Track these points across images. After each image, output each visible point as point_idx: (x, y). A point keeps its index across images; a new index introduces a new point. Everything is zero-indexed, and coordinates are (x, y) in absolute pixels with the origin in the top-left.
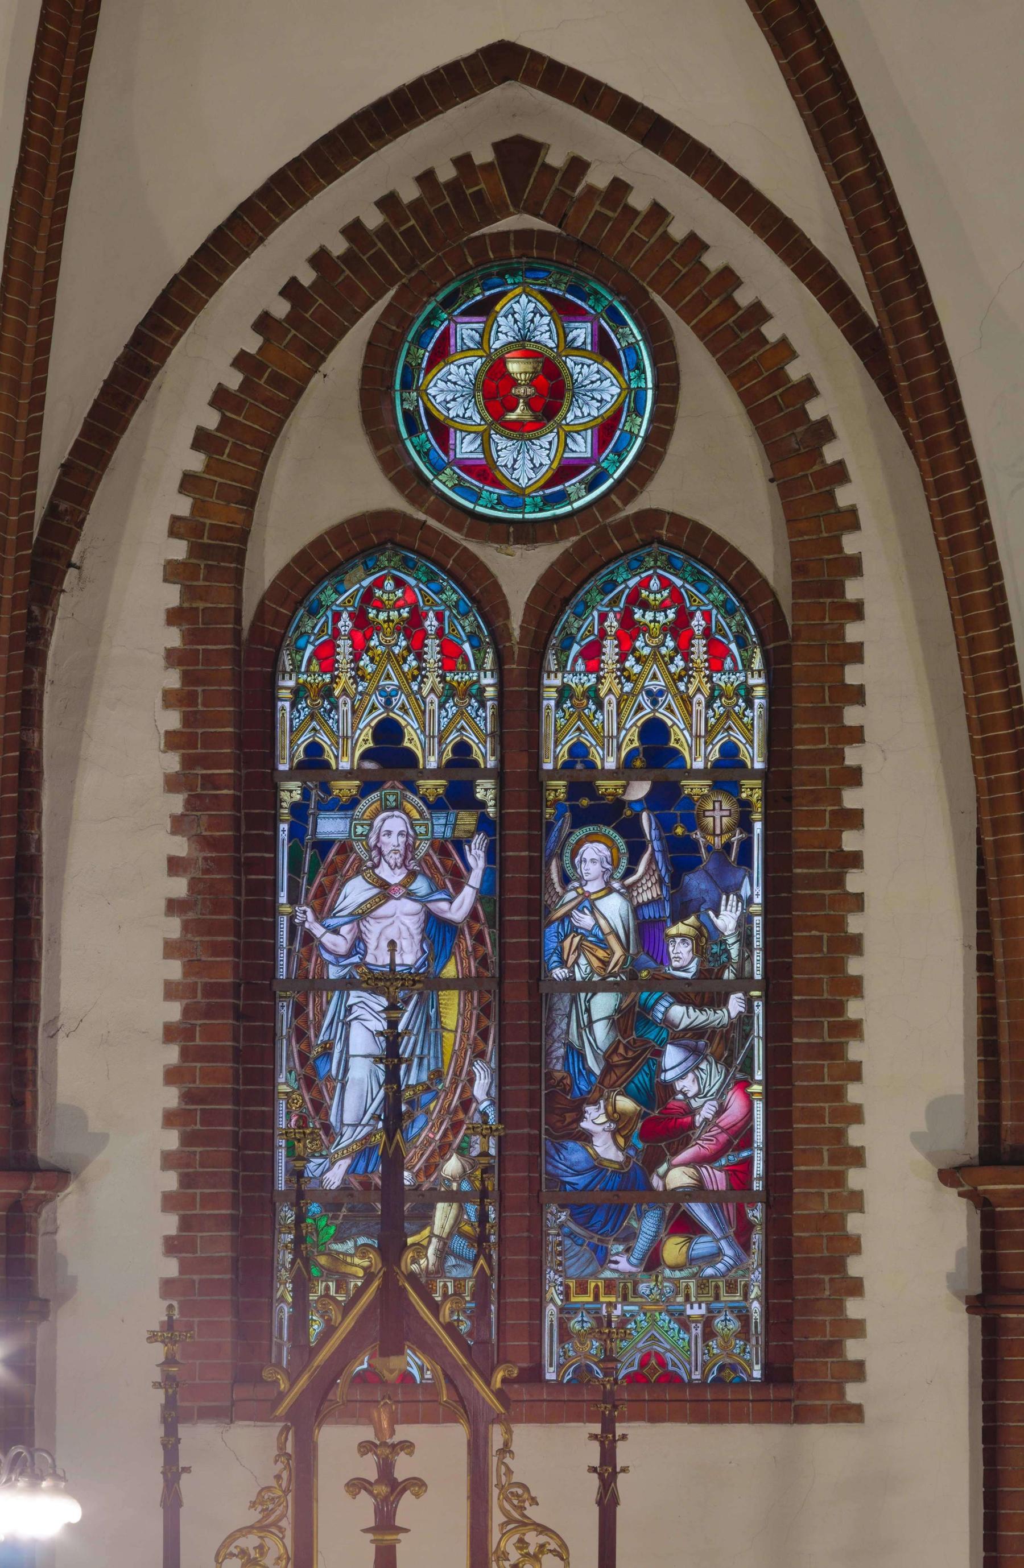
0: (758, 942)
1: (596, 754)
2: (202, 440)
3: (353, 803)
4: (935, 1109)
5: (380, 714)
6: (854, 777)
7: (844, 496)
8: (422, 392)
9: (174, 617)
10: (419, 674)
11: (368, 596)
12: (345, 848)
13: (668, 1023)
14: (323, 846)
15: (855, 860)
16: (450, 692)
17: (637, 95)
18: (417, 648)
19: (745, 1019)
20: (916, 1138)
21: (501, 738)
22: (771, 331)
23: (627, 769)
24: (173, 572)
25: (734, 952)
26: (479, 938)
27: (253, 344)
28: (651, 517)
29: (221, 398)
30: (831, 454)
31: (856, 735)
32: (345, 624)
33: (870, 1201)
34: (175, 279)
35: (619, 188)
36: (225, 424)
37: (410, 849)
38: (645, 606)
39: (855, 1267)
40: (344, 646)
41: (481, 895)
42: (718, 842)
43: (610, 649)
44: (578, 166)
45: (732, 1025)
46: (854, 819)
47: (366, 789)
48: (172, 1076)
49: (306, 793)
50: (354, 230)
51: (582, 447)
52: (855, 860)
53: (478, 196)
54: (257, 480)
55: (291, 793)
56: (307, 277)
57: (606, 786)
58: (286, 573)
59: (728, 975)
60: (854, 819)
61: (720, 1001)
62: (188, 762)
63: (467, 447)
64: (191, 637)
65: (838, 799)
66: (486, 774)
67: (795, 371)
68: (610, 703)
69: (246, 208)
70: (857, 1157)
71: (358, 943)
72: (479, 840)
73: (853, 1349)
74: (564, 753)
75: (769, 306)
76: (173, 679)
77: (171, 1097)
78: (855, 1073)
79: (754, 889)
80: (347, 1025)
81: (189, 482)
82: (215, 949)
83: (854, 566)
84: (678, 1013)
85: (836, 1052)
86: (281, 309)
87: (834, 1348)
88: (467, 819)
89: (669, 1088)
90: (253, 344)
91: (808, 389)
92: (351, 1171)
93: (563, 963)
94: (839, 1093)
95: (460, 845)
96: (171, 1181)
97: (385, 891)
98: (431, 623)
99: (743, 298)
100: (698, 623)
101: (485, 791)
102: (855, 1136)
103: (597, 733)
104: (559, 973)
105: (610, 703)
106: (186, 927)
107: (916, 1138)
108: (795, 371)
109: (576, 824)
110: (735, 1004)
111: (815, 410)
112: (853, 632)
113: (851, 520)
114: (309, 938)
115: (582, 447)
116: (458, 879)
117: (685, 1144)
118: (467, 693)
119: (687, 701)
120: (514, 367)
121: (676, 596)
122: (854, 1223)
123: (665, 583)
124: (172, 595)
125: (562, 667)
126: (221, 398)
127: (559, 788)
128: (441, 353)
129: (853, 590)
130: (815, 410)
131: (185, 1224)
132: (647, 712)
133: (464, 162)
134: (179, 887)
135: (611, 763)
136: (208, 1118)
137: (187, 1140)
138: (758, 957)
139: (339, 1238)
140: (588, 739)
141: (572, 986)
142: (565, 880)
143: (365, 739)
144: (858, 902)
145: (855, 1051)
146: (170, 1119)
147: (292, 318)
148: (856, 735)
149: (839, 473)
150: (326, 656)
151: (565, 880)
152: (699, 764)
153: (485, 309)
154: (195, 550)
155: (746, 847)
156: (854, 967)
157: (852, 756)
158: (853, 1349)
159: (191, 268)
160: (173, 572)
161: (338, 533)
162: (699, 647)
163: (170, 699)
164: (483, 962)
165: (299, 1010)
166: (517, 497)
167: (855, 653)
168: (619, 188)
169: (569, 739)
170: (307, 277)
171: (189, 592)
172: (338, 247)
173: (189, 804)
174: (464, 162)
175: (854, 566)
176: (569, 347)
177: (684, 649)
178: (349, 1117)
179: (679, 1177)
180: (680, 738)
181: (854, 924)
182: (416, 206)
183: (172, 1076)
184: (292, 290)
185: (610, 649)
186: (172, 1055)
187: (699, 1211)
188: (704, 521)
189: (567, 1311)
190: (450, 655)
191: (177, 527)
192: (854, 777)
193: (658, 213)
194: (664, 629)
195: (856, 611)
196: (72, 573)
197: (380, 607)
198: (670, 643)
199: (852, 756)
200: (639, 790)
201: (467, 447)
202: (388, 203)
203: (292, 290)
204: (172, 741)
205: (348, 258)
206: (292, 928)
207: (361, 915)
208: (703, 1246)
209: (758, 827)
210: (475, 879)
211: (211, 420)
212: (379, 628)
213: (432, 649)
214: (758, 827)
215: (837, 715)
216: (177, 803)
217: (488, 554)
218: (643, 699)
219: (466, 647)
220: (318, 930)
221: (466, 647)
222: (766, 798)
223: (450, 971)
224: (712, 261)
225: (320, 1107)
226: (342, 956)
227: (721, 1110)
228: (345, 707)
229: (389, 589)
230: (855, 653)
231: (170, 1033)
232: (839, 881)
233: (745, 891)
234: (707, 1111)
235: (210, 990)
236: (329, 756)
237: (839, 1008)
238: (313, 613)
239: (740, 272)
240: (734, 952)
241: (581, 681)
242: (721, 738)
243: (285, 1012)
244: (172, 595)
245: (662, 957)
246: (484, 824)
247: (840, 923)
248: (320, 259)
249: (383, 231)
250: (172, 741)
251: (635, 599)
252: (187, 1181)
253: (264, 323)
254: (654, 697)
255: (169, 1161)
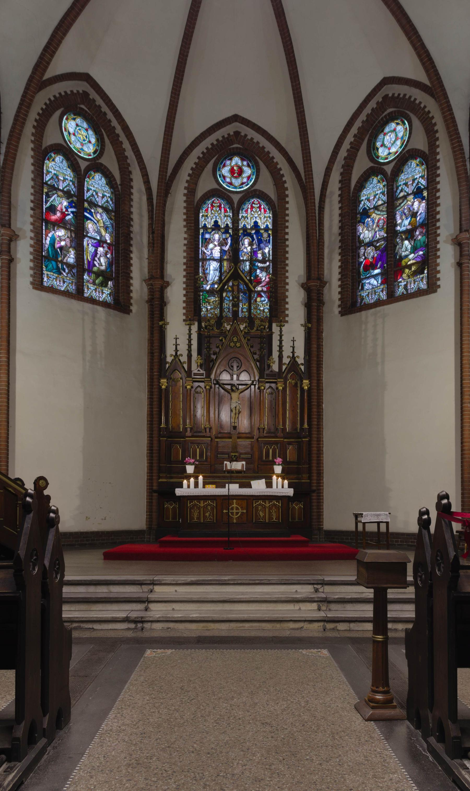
0: (271, 254)
1: (247, 226)
2: (189, 175)
3: (211, 233)
4: (299, 277)
5: (215, 219)
6: (287, 227)
7: (286, 185)
8: (221, 171)
9: (185, 202)
10: (220, 213)
11: (213, 202)
12: (210, 239)
13: (258, 266)
14: (206, 239)
15: (287, 240)
16: (225, 216)
17: (256, 123)
18: (220, 209)
19: (269, 265)
20: (296, 281)
21: (233, 223)
22: (275, 161)
23: (252, 229)
24: (185, 195)
25: (267, 255)
26: (229, 253)
27: (197, 161)
28: (256, 190)
29: (192, 169)
30: (284, 179)
31: (288, 221)
32: (210, 206)
33: (289, 290)
34: (186, 149)
35: (252, 139)
36: (193, 173)
37: (219, 239)
38: (254, 204)
39: (287, 300)
40: (209, 209)
41: (230, 246)
42: (265, 239)
43: (249, 210)
44: (246, 135)
45: (267, 266)
46: (287, 233)
47: (212, 231)
48: (185, 270)
49: (204, 231)
50: (212, 144)
51: (245, 180)
52: (287, 240)
53: (231, 140)
54: (197, 181)
55: (201, 231)
56: (205, 151)
57: (249, 231)
58: (201, 197)
59: (267, 259)
60: (287, 233)
61: (265, 263)
62: (187, 223)
63: (228, 180)
64: (187, 205)
65: (285, 230)
66: (231, 228)
67: (279, 167)
68: (249, 218)
69: (197, 138)
70: (287, 284)
71: (212, 253)
72: (230, 238)
73: (287, 312)
74: (242, 226)
75: (274, 157)
76: (185, 211)
77: (184, 273)
78: (287, 271)
79: (270, 246)
80: (210, 265)
81: (187, 181)
82: (191, 251)
83: (287, 196)
84: (259, 264)
85: (285, 268)
86: (201, 156)
87: (284, 312)
88: (228, 235)
89: (258, 276)
90: (197, 161)
91: (280, 169)
92: (210, 287)
93: (242, 257)
94: (285, 274)
95: (227, 239)
96: (184, 286)
97: (215, 246)
98: (223, 206)
99: (271, 155)
100: (262, 207)
101: (230, 231)
102: (287, 281)
103: (248, 223)
104: (241, 258)
105: (249, 218)
106: (187, 248)
107: (296, 281)
108: (279, 167)
109: (244, 236)
110: (268, 264)
111: (281, 172)
112: (287, 206)
113: (287, 189)
114: (204, 253)
115: (245, 180)
116: (227, 244)
117: (261, 284)
118: (228, 216)
119: (261, 218)
120: (235, 168)
121: (259, 203)
122: (287, 293)
123: (257, 201)
124: (185, 198)
125: (242, 213)
126: (192, 169)
127: (241, 232)
128: (224, 166)
129: (287, 199)
130: (281, 172)
131: (187, 292)
132: (255, 220)
133: (229, 134)
134: (186, 242)
135: (249, 227)
136: (190, 276)
137: (187, 280)
138: (271, 257)
139: (208, 297)
140: (246, 224)
141: (243, 261)
142: (242, 245)
143: (212, 223)
144: (288, 246)
145: (287, 268)
146: (184, 276)
147: (203, 157)
148: (288, 221)
149: (285, 182)
150: (207, 210)
151: (242, 245)
152: (262, 228)
153: (231, 159)
154: (188, 192)
155: (269, 240)
156: (287, 255)
157: (287, 224)
158: (287, 312)
159: (189, 147)
160: (185, 195)
161: (209, 192)
162: (263, 210)
163: (184, 214)
164: (230, 256)
165: (203, 263)
166: (235, 187)
167: (287, 209)
168: (252, 139)
169: (243, 224)
170: (205, 151)
171: (187, 198)
172: (210, 147)
173: (187, 229)
174: (229, 134)
175: (287, 196)
176: (243, 165)
177: (260, 210)
178: (210, 279)
179: (259, 289)
180: (260, 224)
181: (287, 249)
182: (222, 141)
183: (185, 270)
184: (203, 153)
185: (249, 210)
186: (185, 267)
187: (263, 294)
188: (264, 191)
189: (242, 309)
190: (226, 211)
191: (185, 188)
192: (287, 227)
193: (258, 143)
194: (257, 208)
195: (288, 202)
196: (170, 195)
197: (215, 203)
198: (258, 209)
199: (287, 224)
200: (253, 232)
201: (228, 180)
202: (217, 140)
203: (203, 153)
204: (185, 220)
205: (211, 148)
206: (202, 251)
207: (212, 249)
208: (263, 299)
209: (271, 237)
210: (229, 244)
211: (191, 172)
212: (215, 207)
213: (223, 210)
214: (271, 237)
215: (285, 218)
216: (185, 229)
217: (231, 195)
218: (254, 218)
219: (228, 210)
220: (205, 251)
221: (228, 210)
222: (272, 233)
223: (225, 258)
224: (266, 150)
225: (206, 277)
226: (230, 202)
227: (266, 279)
228: (210, 218)
229: (216, 201)
230: (287, 209)
231: (184, 264)
232: (285, 243)
233: (269, 247)
234: (264, 279)
235: (190, 257)
236: (207, 225)
237: (285, 262)
238: (205, 204)
239: (270, 152)
240: (267, 255)
241: (245, 215)
242: (266, 224)
243: (201, 264)
244: (185, 198)
245: (257, 256)
246: (230, 236)
247: (285, 249)
248: (207, 148)
249: (217, 144)
250: (185, 220)
251: (253, 203)
252: (187, 286)
253: (199, 158)
254: (256, 218)
255: (184, 283)
